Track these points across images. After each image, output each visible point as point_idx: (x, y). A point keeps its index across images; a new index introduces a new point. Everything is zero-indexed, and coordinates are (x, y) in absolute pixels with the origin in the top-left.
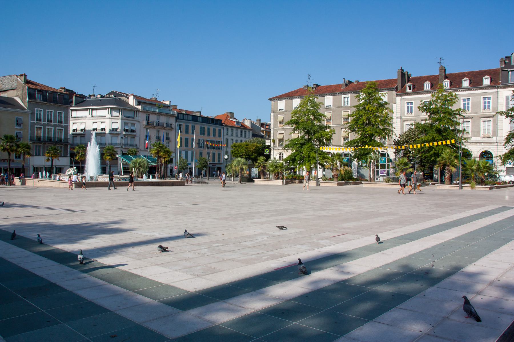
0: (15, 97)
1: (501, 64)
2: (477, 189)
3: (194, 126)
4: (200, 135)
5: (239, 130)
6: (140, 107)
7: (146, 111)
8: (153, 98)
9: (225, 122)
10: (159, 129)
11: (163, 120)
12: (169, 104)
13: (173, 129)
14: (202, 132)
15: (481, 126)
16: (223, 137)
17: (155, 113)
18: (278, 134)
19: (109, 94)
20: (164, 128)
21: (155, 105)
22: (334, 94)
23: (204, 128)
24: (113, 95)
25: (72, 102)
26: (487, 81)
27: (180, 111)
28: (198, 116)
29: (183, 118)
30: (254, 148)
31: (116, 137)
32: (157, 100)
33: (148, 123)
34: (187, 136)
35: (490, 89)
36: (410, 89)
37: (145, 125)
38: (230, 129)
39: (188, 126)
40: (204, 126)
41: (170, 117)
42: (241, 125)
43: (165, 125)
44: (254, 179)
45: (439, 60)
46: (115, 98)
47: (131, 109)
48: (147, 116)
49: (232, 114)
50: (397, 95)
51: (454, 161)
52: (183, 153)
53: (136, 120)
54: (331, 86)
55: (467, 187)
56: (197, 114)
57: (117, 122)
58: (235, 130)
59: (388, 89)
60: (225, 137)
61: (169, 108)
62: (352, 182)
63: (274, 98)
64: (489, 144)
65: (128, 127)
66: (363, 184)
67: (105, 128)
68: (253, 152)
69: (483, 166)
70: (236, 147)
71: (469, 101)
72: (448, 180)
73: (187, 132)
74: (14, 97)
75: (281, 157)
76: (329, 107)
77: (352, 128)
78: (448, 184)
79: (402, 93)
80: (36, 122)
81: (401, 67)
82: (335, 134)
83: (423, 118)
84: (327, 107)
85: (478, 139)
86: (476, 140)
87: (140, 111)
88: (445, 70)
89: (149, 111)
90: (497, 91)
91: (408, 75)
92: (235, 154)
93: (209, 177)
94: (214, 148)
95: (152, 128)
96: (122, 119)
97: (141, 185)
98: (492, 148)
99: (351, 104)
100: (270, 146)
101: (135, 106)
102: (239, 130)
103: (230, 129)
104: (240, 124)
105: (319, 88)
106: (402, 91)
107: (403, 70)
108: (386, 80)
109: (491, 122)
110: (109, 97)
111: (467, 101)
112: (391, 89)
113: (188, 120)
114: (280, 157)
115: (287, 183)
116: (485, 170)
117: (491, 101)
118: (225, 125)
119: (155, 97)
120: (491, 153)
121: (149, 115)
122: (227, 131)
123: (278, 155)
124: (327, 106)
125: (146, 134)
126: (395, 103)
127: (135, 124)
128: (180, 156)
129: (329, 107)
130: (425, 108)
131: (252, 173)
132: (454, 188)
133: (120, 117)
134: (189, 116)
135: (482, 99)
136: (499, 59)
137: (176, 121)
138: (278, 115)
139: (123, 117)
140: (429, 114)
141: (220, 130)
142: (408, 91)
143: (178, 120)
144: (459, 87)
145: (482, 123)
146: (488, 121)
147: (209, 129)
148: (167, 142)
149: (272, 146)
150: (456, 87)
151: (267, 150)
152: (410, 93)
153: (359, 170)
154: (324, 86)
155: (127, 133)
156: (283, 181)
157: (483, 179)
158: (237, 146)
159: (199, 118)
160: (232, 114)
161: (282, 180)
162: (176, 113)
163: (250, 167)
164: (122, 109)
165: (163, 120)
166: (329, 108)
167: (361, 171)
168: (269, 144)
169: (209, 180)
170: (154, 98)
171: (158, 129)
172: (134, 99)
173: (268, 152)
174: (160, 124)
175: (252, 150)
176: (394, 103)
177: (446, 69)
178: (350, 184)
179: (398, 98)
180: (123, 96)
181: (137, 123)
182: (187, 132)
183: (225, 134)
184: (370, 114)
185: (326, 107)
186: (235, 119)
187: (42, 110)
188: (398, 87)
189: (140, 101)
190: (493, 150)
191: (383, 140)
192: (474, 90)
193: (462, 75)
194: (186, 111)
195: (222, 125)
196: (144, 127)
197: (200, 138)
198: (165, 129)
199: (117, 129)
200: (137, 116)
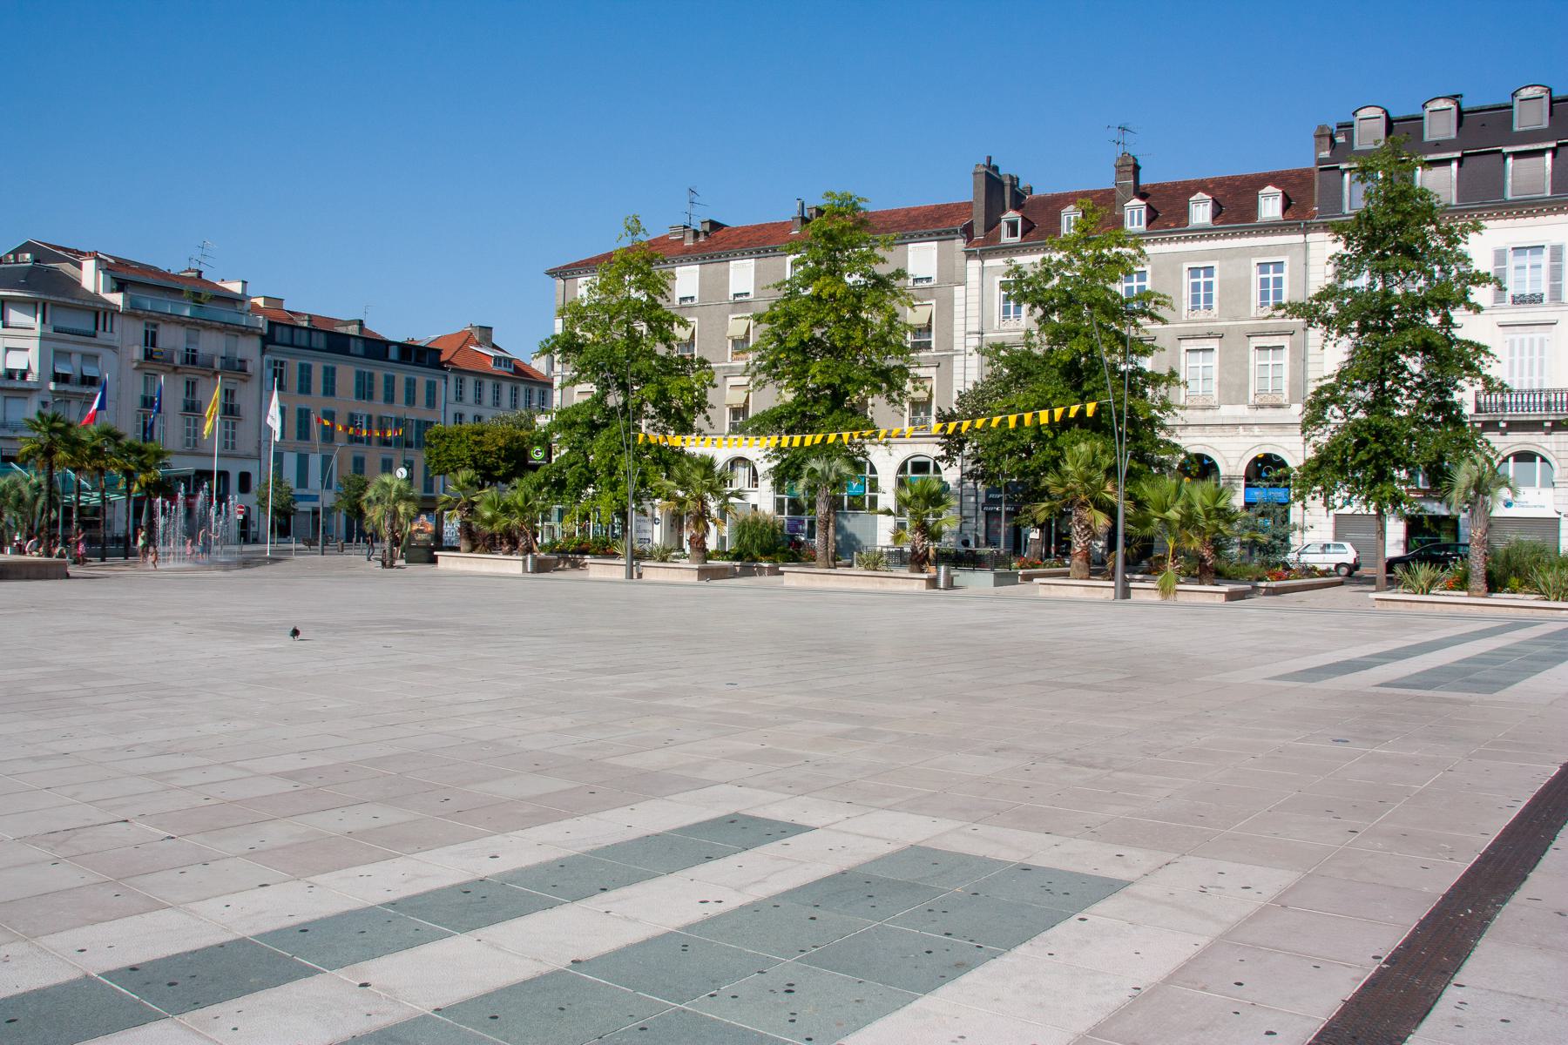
1: (1319, 147)
2: (1181, 598)
3: (333, 369)
4: (354, 400)
5: (506, 388)
6: (117, 299)
7: (140, 312)
8: (190, 270)
9: (453, 356)
10: (196, 377)
11: (211, 345)
12: (240, 292)
13: (250, 376)
14: (364, 389)
15: (1251, 367)
16: (443, 408)
17: (180, 321)
18: (576, 393)
19: (16, 252)
21: (181, 291)
22: (759, 252)
23: (371, 375)
24: (28, 256)
26: (1270, 206)
27: (292, 319)
28: (348, 336)
30: (501, 442)
31: (23, 400)
32: (204, 277)
33: (149, 356)
34: (304, 402)
35: (1281, 234)
36: (1014, 234)
37: (138, 361)
38: (470, 382)
39: (310, 367)
40: (372, 371)
41: (239, 334)
42: (512, 370)
43: (217, 364)
44: (436, 553)
45: (1115, 134)
47: (91, 304)
48: (147, 332)
49: (486, 331)
50: (970, 255)
51: (1104, 488)
52: (291, 461)
53: (101, 342)
54: (761, 227)
55: (1145, 591)
56: (350, 327)
57: (27, 350)
58: (488, 385)
59: (939, 234)
60: (454, 408)
61: (239, 306)
62: (766, 565)
63: (565, 267)
64: (1277, 431)
65: (70, 367)
66: (782, 573)
68: (499, 457)
69: (1204, 507)
70: (443, 437)
71: (1212, 276)
72: (1081, 560)
73: (305, 388)
76: (744, 298)
77: (771, 369)
78: (1081, 579)
79: (986, 247)
81: (989, 159)
82: (715, 386)
83: (1019, 327)
84: (737, 299)
85: (1241, 412)
86: (1235, 418)
87: (118, 311)
88: (1136, 168)
89: (154, 314)
90: (1305, 242)
91: (1013, 186)
92: (438, 461)
93: (323, 545)
94: (386, 443)
95: (208, 377)
96: (43, 338)
97: (28, 578)
98: (1286, 446)
102: (506, 388)
103: (470, 382)
104: (510, 367)
105: (719, 234)
106: (986, 241)
107: (996, 169)
108: (944, 206)
109: (1286, 353)
110: (17, 262)
111: (1205, 276)
112: (948, 233)
113: (310, 348)
115: (541, 567)
116: (1210, 523)
117: (1285, 275)
118: (451, 366)
119: (195, 266)
120: (1283, 464)
121: (155, 326)
122: (461, 387)
124: (736, 295)
125: (142, 393)
126: (963, 283)
127: (97, 357)
128: (279, 469)
129: (744, 298)
130: (1021, 291)
131: (446, 530)
132: (1103, 590)
133: (38, 331)
134: (314, 334)
135: (1255, 270)
136: (1314, 130)
137: (264, 351)
139: (50, 331)
140: (1039, 312)
141: (431, 388)
142: (1006, 239)
143: (269, 347)
144: (1176, 226)
145: (1253, 356)
146: (1274, 348)
147: (390, 381)
148: (227, 423)
150: (1167, 227)
151: (538, 448)
152: (1013, 247)
153: (840, 519)
154: (737, 228)
155: (63, 387)
156: (525, 561)
157: (1205, 561)
158: (444, 436)
159: (352, 341)
160: (486, 331)
161: (521, 558)
162: (261, 322)
164: (44, 306)
165: (211, 345)
166: (741, 302)
167: (845, 523)
169: (323, 554)
171: (191, 376)
172: (97, 269)
173: (541, 455)
174: (199, 360)
175: (494, 449)
177: (1139, 164)
178: (761, 571)
179: (974, 265)
180: (65, 260)
181: (107, 355)
182: (305, 388)
183: (452, 396)
184: (828, 314)
185: (731, 298)
186: (494, 347)
188: (975, 226)
189: (121, 275)
190: (1289, 451)
191: (922, 414)
192: (1221, 238)
193: (1189, 189)
194: (310, 316)
195: (440, 366)
196: (136, 369)
197: (355, 412)
198: (180, 370)
199: (24, 374)
200: (108, 329)
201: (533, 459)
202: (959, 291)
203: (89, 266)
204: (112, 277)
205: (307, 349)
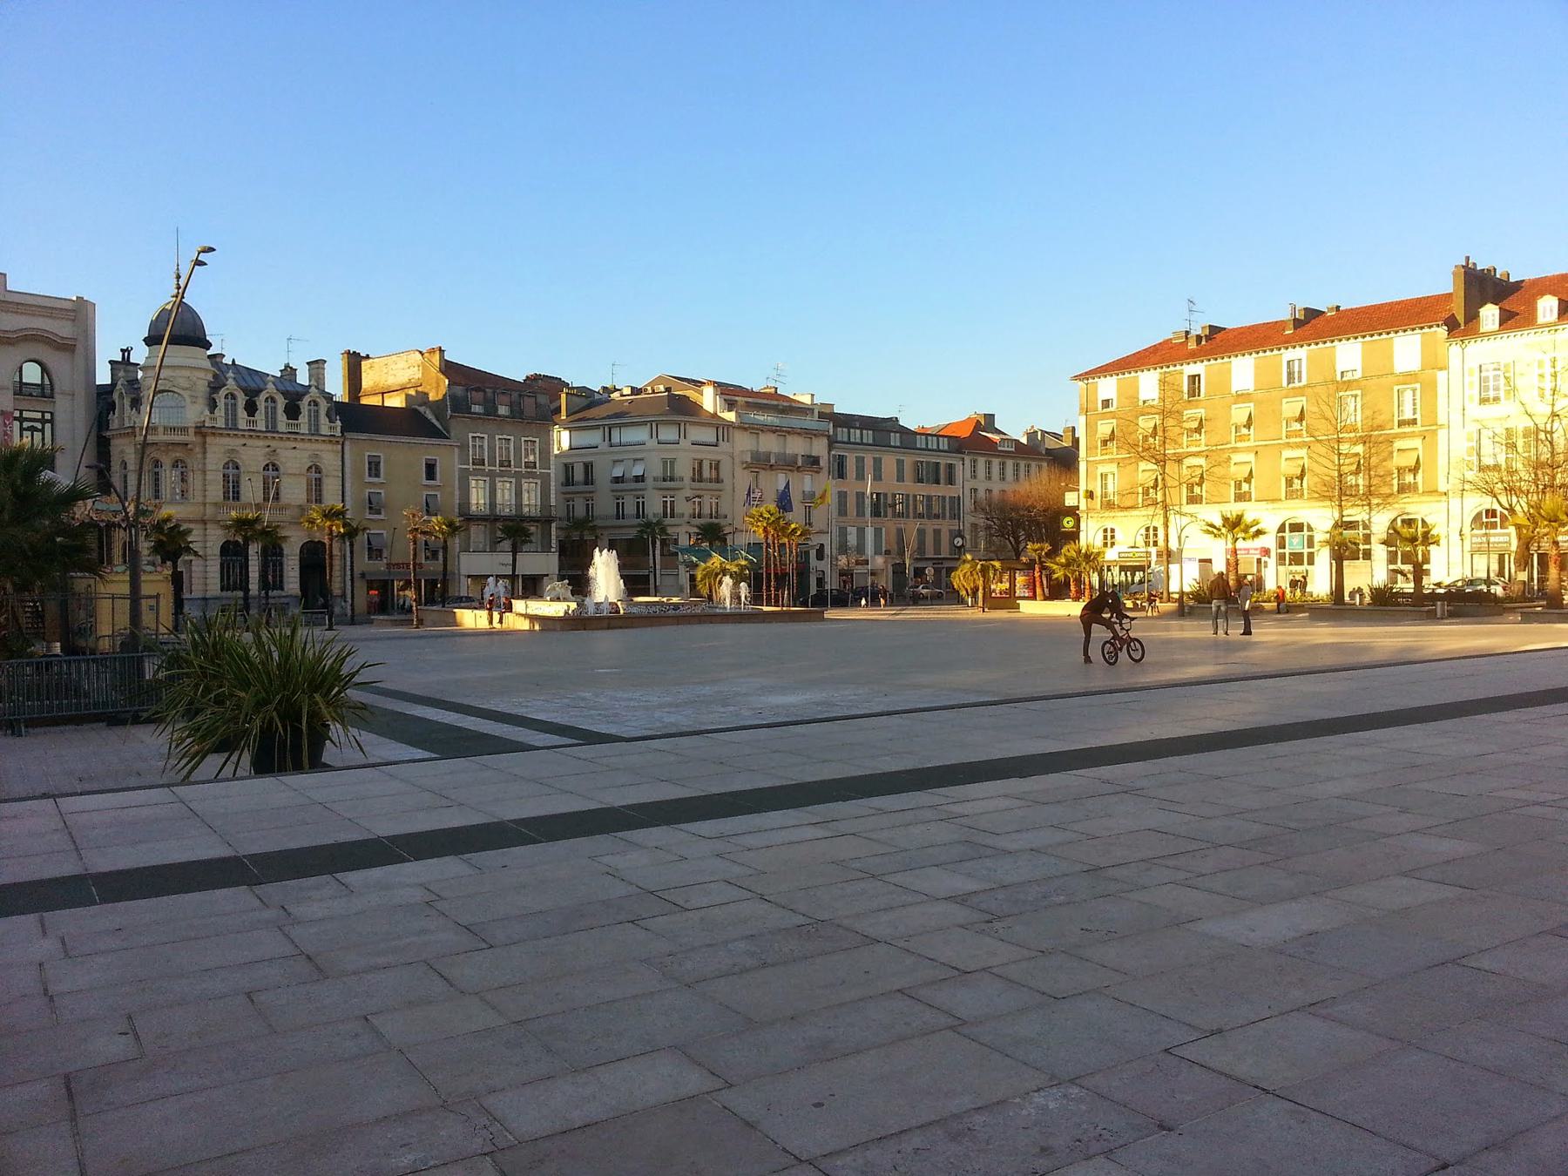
0: (420, 405)
3: (880, 459)
6: (730, 416)
20: (799, 467)
25: (558, 410)
29: (927, 439)
32: (779, 392)
46: (666, 394)
49: (990, 418)
60: (968, 486)
67: (643, 475)
74: (416, 407)
75: (1109, 538)
80: (471, 467)
99: (1308, 381)
100: (1077, 508)
101: (719, 414)
105: (1218, 336)
113: (927, 449)
114: (1105, 538)
123: (1101, 535)
138: (1099, 422)
149: (1083, 507)
154: (1234, 330)
160: (990, 418)
163: (1010, 569)
168: (1076, 504)
170: (771, 388)
173: (1071, 524)
176: (1441, 369)
179: (1455, 350)
187: (486, 436)
196: (745, 468)
201: (1064, 527)
202: (1441, 376)
203: (708, 391)
204: (725, 400)
205: (847, 443)
